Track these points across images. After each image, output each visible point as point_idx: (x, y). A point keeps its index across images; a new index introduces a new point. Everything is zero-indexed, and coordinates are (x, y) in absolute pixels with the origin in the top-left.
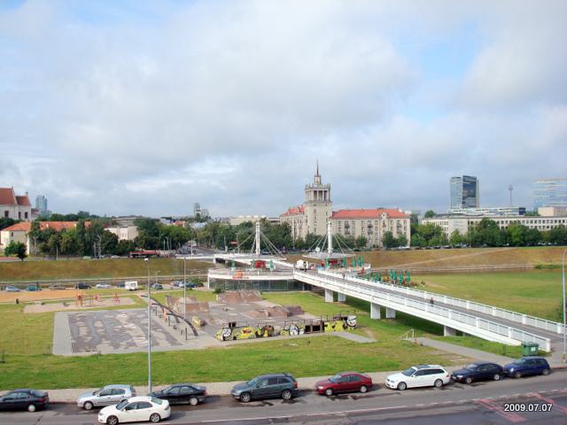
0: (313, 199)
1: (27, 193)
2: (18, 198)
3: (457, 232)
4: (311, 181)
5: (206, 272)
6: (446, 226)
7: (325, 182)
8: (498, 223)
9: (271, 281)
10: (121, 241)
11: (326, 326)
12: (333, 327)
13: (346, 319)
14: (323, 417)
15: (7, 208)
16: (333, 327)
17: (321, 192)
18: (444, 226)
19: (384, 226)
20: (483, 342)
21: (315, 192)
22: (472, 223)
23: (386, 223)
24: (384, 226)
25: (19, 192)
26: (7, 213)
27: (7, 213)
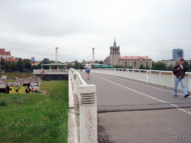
0: (173, 86)
1: (10, 51)
2: (6, 52)
3: (171, 66)
4: (112, 45)
5: (32, 71)
6: (167, 64)
7: (117, 46)
8: (188, 63)
9: (50, 75)
10: (33, 66)
11: (11, 89)
12: (17, 91)
13: (28, 85)
14: (78, 132)
15: (2, 56)
16: (17, 91)
17: (116, 49)
18: (166, 64)
19: (141, 63)
20: (65, 105)
21: (113, 49)
22: (177, 62)
23: (142, 62)
24: (141, 63)
25: (6, 50)
26: (2, 57)
27: (2, 57)
